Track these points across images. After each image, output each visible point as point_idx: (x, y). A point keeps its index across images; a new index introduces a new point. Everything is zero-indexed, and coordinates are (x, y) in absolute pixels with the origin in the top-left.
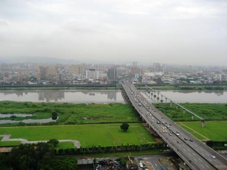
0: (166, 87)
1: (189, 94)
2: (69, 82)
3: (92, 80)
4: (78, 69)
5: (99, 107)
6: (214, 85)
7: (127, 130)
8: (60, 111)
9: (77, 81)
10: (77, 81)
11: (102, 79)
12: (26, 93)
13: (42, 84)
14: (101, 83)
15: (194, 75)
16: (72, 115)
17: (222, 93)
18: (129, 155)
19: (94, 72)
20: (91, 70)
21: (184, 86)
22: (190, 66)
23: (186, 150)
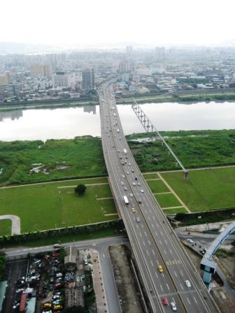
0: (162, 97)
1: (193, 104)
2: (27, 96)
3: (58, 88)
4: (42, 69)
5: (59, 146)
6: (151, 96)
7: (85, 193)
8: (5, 159)
9: (38, 94)
10: (38, 94)
11: (73, 88)
12: (18, 118)
13: (6, 101)
14: (72, 95)
15: (208, 71)
16: (21, 166)
17: (19, 115)
18: (69, 245)
19: (63, 76)
20: (58, 73)
21: (188, 91)
22: (208, 51)
23: (155, 225)
